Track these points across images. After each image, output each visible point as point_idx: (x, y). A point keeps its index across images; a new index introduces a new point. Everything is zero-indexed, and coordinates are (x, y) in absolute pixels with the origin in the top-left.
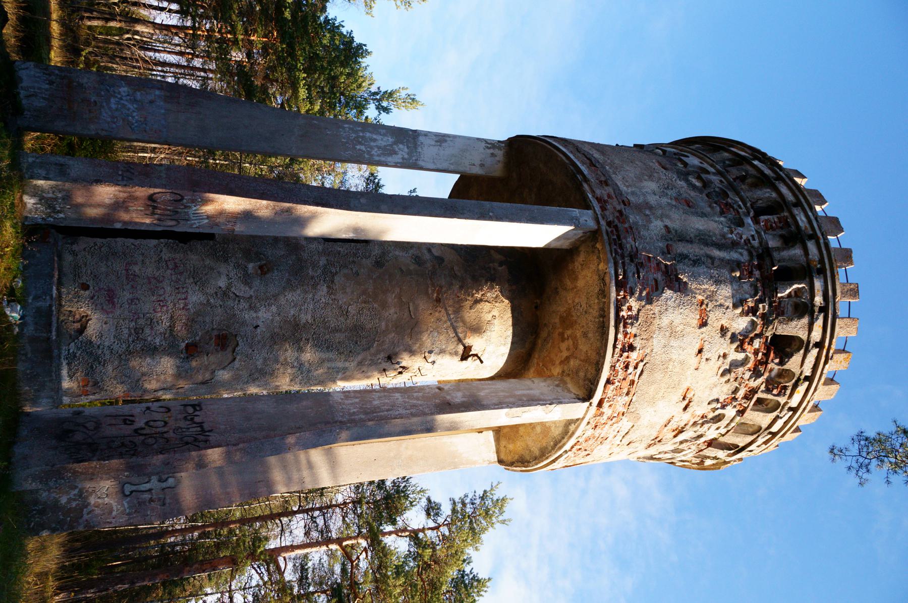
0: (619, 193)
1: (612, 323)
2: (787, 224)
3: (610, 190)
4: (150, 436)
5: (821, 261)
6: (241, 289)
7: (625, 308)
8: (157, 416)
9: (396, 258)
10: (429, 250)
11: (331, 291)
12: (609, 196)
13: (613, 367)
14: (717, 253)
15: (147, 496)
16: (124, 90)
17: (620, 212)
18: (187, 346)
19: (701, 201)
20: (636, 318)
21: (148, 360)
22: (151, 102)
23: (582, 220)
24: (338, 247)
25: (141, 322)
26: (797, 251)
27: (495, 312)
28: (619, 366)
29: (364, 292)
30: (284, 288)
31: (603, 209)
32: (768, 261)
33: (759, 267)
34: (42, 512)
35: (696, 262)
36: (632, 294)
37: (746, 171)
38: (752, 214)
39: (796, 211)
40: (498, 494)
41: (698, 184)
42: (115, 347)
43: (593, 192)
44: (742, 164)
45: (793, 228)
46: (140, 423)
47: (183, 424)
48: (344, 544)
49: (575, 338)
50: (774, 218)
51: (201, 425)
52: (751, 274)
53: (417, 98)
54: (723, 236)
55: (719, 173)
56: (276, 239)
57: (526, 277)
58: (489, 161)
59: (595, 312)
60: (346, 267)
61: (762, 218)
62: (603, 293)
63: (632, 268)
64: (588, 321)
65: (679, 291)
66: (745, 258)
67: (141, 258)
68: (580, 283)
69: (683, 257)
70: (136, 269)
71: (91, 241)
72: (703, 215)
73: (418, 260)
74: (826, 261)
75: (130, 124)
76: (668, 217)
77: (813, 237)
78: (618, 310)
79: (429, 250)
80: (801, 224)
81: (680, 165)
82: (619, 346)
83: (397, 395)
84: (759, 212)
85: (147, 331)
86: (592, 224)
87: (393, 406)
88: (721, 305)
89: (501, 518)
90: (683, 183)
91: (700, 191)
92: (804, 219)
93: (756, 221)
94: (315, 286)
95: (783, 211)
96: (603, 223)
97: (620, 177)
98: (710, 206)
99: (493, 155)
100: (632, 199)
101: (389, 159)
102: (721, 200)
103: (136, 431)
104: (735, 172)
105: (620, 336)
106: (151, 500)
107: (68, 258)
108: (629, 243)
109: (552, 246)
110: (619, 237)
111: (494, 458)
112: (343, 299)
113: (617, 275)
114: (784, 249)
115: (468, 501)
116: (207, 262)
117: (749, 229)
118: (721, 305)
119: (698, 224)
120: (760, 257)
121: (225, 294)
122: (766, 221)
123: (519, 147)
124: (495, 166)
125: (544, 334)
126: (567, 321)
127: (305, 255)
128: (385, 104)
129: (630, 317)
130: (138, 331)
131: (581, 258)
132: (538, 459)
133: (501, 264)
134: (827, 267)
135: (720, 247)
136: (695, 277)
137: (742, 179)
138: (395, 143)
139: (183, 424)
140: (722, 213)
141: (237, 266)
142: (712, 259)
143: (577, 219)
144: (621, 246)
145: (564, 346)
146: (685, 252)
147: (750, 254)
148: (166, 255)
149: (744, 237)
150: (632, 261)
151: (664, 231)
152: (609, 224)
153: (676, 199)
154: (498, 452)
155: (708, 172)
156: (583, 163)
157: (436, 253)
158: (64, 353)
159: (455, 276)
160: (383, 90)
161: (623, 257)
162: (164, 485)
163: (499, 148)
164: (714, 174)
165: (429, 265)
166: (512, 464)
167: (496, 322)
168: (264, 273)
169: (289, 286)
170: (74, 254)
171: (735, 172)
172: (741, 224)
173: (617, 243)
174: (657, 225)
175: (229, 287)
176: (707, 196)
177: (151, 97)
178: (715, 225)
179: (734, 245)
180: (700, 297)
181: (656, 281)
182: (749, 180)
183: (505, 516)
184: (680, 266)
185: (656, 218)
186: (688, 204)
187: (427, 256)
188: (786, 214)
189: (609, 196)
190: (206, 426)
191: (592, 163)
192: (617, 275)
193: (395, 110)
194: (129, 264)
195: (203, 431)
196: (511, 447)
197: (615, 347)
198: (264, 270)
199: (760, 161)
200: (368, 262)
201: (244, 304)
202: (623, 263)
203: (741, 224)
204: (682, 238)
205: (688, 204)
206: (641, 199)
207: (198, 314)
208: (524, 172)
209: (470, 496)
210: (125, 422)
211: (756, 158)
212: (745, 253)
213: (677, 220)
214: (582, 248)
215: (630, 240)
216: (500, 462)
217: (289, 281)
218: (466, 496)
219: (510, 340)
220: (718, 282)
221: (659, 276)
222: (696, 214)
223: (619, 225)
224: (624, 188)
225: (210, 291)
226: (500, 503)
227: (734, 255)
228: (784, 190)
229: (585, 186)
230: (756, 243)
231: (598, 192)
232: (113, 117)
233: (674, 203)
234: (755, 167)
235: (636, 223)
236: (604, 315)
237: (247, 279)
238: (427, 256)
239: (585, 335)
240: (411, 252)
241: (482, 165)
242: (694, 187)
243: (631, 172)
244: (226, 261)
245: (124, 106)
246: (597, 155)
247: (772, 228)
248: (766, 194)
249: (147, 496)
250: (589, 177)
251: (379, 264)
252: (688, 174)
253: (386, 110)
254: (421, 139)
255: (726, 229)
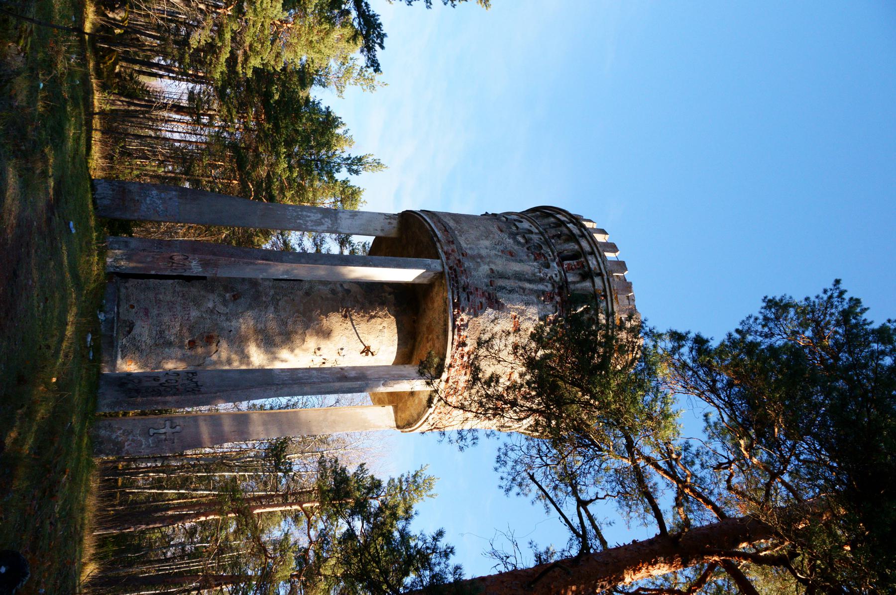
0: (460, 248)
1: (450, 328)
2: (583, 266)
3: (454, 247)
4: (168, 387)
5: (605, 290)
6: (222, 309)
7: (458, 319)
8: (172, 378)
9: (319, 290)
10: (341, 285)
11: (276, 310)
12: (453, 251)
13: (453, 356)
14: (527, 285)
15: (163, 437)
16: (154, 192)
17: (459, 261)
18: (189, 342)
19: (522, 252)
20: (466, 325)
21: (167, 350)
22: (170, 199)
23: (433, 266)
24: (283, 284)
25: (164, 327)
26: (587, 284)
27: (385, 324)
28: (457, 356)
29: (298, 311)
30: (248, 309)
31: (448, 258)
32: (565, 291)
33: (560, 294)
34: (101, 443)
35: (511, 291)
36: (463, 311)
37: (561, 232)
38: (557, 260)
39: (589, 258)
40: (426, 473)
41: (522, 241)
42: (148, 341)
43: (442, 248)
44: (560, 226)
45: (586, 269)
46: (163, 380)
47: (187, 382)
48: (304, 505)
49: (432, 339)
50: (574, 263)
51: (196, 383)
52: (552, 299)
53: (382, 162)
54: (534, 275)
55: (541, 233)
56: (243, 279)
57: (406, 304)
58: (387, 227)
59: (442, 323)
60: (286, 295)
61: (566, 262)
62: (445, 311)
63: (463, 296)
64: (438, 329)
65: (499, 309)
66: (549, 288)
67: (163, 291)
68: (436, 305)
69: (502, 288)
70: (161, 297)
71: (135, 281)
72: (521, 261)
73: (333, 292)
74: (608, 290)
75: (157, 212)
76: (494, 263)
77: (600, 274)
78: (454, 320)
79: (341, 285)
80: (591, 266)
81: (514, 228)
82: (456, 343)
83: (314, 372)
84: (563, 258)
85: (167, 332)
86: (439, 268)
87: (310, 377)
88: (530, 319)
89: (429, 493)
90: (511, 241)
91: (522, 245)
92: (595, 263)
93: (560, 264)
94: (266, 307)
95: (581, 257)
96: (447, 268)
97: (463, 238)
98: (528, 256)
99: (390, 223)
100: (468, 252)
101: (319, 228)
102: (536, 252)
103: (161, 384)
104: (553, 232)
105: (456, 337)
106: (166, 440)
107: (123, 290)
108: (463, 280)
109: (417, 281)
110: (456, 276)
111: (394, 424)
112: (283, 315)
113: (453, 300)
114: (578, 282)
115: (404, 479)
116: (202, 293)
117: (554, 270)
118: (530, 319)
119: (516, 267)
120: (561, 288)
121: (212, 311)
122: (569, 264)
123: (407, 218)
124: (392, 230)
125: (419, 339)
126: (430, 330)
127: (261, 289)
128: (355, 167)
129: (462, 325)
130: (161, 332)
131: (436, 289)
132: (416, 421)
133: (390, 294)
134: (608, 294)
135: (530, 281)
136: (510, 301)
137: (559, 236)
138: (323, 218)
139: (187, 382)
140: (535, 260)
141: (220, 295)
142: (524, 289)
143: (429, 265)
144: (457, 282)
145: (428, 345)
146: (503, 285)
147: (553, 286)
148: (178, 289)
149: (549, 275)
150: (464, 290)
151: (489, 272)
152: (450, 268)
153: (502, 251)
154: (396, 421)
155: (531, 232)
156: (440, 230)
157: (346, 286)
158: (120, 344)
159: (357, 302)
160: (353, 156)
161: (458, 288)
162: (174, 430)
163: (394, 219)
164: (536, 234)
165: (340, 295)
166: (403, 427)
167: (385, 330)
168: (235, 299)
169: (250, 307)
170: (127, 288)
171: (553, 232)
172: (548, 266)
173: (455, 279)
174: (484, 269)
175: (214, 307)
176: (528, 249)
177: (170, 196)
178: (529, 268)
179: (542, 280)
180: (514, 314)
181: (481, 303)
182: (564, 237)
183: (432, 492)
184: (499, 294)
185: (485, 264)
186: (511, 254)
187: (339, 289)
188: (583, 259)
189: (453, 251)
190: (199, 383)
191: (446, 229)
192: (453, 300)
193: (363, 173)
194: (157, 294)
195: (197, 386)
196: (403, 416)
197: (452, 344)
198: (235, 298)
199: (574, 224)
200: (300, 293)
201: (223, 318)
202: (458, 293)
203: (548, 266)
204: (502, 276)
205: (511, 254)
206: (476, 252)
207: (196, 323)
208: (409, 235)
209: (405, 476)
210: (154, 380)
211: (572, 222)
212: (550, 285)
213: (500, 265)
214: (436, 284)
215: (464, 278)
216: (398, 427)
217: (250, 304)
218: (402, 476)
219: (396, 342)
220: (527, 304)
221: (483, 300)
222: (516, 261)
223: (457, 269)
224: (464, 245)
225: (203, 309)
226: (429, 482)
227: (541, 287)
228: (584, 244)
229: (438, 245)
230: (557, 279)
231: (445, 248)
232: (148, 208)
233: (500, 254)
234: (568, 228)
235: (469, 267)
236: (446, 325)
237: (225, 303)
238: (339, 289)
239: (438, 338)
240: (329, 286)
241: (382, 230)
242: (519, 243)
243: (473, 234)
244: (213, 292)
245: (154, 202)
246: (452, 224)
247: (572, 269)
248: (573, 246)
249: (163, 437)
250: (441, 238)
251: (307, 294)
252: (517, 234)
253: (357, 172)
254: (340, 215)
255: (536, 270)
